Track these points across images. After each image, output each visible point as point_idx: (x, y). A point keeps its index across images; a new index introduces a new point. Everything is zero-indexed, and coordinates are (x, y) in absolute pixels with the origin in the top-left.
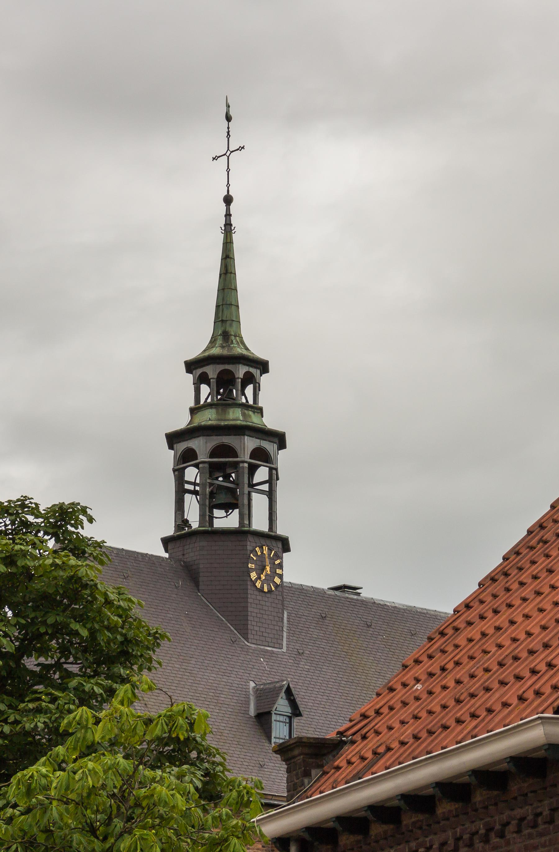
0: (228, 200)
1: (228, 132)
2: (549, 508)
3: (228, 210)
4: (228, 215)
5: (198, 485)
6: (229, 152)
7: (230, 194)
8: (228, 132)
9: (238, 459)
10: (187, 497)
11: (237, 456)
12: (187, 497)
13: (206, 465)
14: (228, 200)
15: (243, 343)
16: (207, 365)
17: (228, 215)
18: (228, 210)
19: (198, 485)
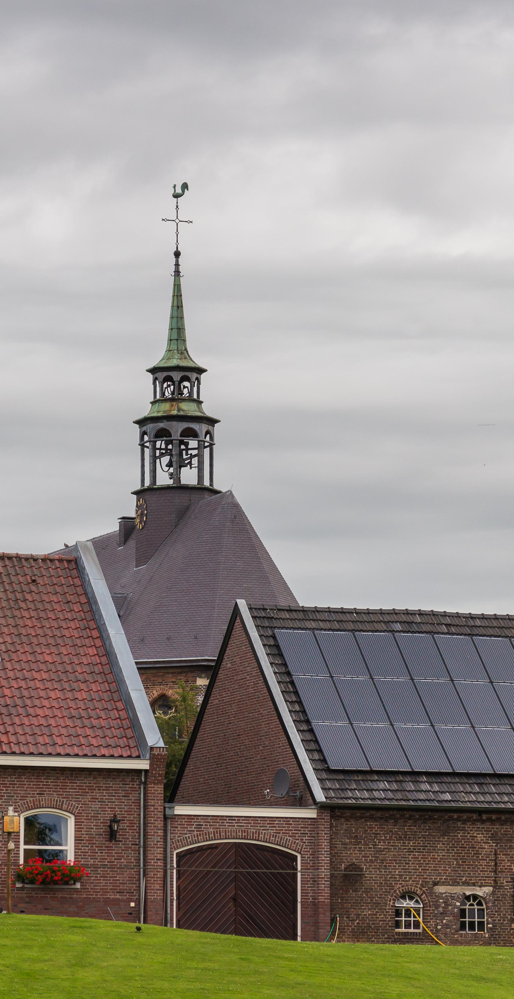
0: (177, 254)
1: (177, 206)
2: (113, 527)
3: (177, 261)
4: (177, 265)
5: (163, 449)
6: (177, 221)
7: (179, 249)
8: (177, 206)
9: (172, 438)
10: (145, 449)
11: (171, 436)
12: (145, 449)
13: (178, 442)
14: (177, 254)
15: (191, 360)
16: (173, 371)
17: (177, 265)
18: (177, 261)
19: (163, 449)
